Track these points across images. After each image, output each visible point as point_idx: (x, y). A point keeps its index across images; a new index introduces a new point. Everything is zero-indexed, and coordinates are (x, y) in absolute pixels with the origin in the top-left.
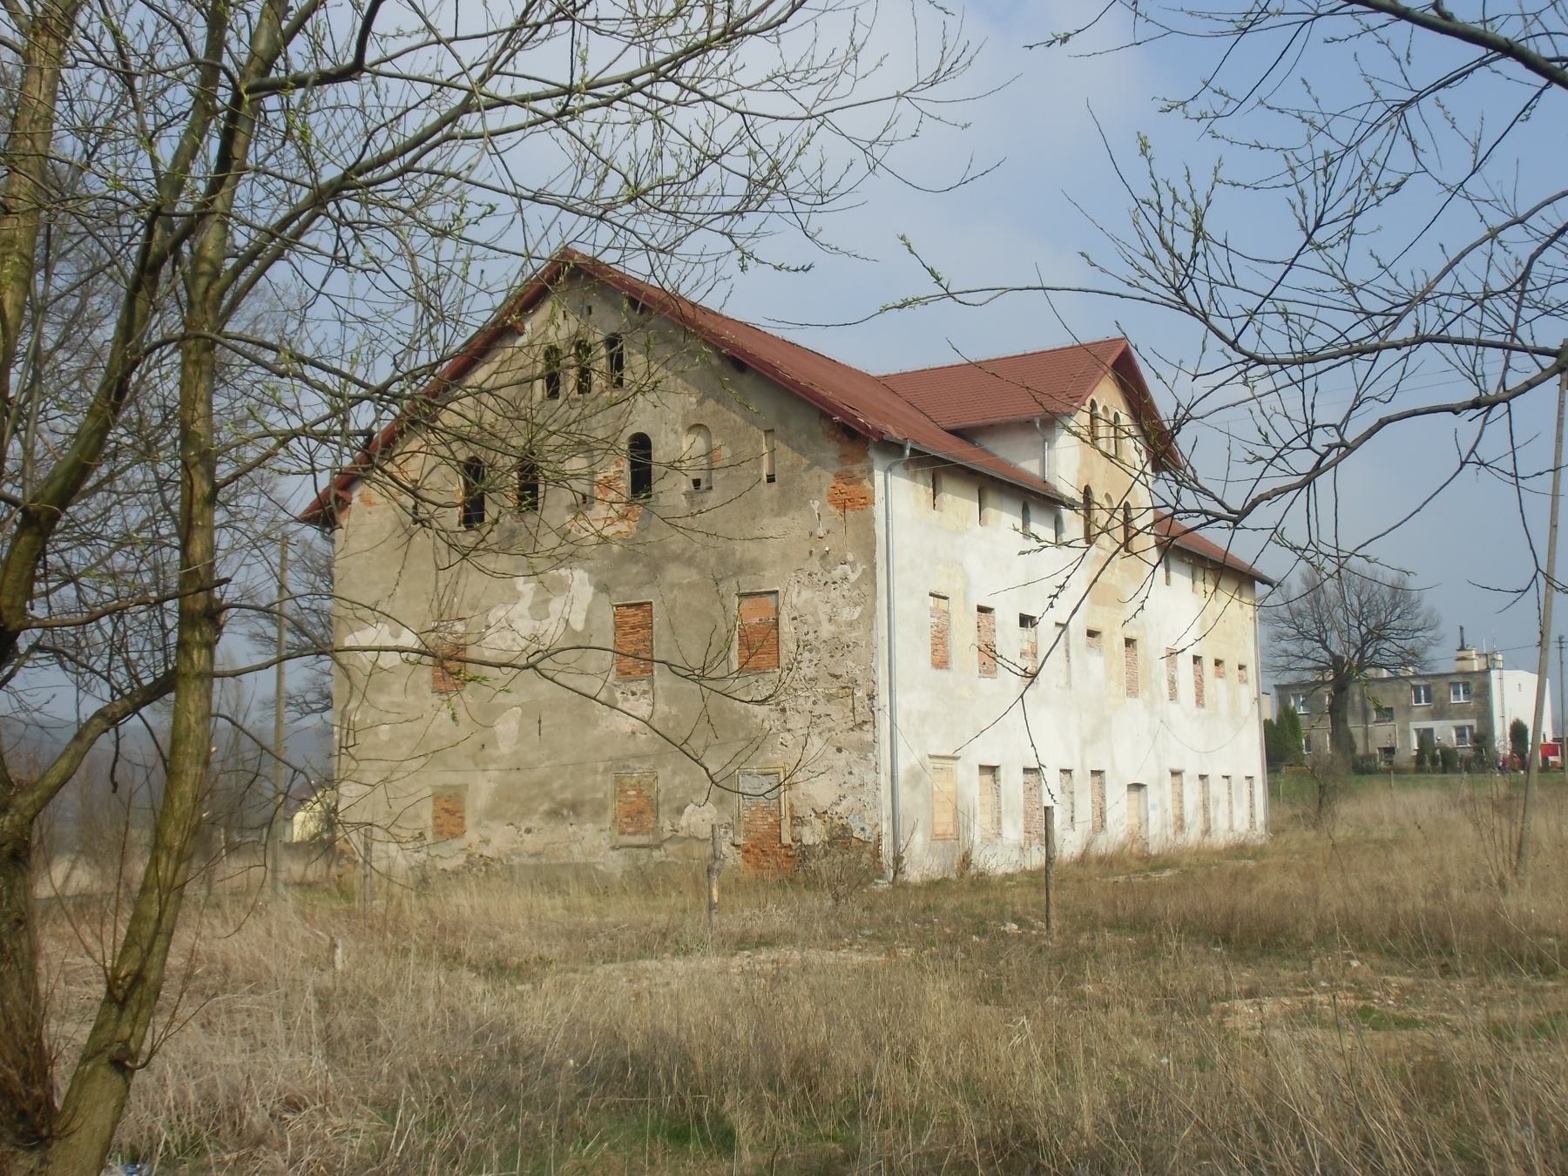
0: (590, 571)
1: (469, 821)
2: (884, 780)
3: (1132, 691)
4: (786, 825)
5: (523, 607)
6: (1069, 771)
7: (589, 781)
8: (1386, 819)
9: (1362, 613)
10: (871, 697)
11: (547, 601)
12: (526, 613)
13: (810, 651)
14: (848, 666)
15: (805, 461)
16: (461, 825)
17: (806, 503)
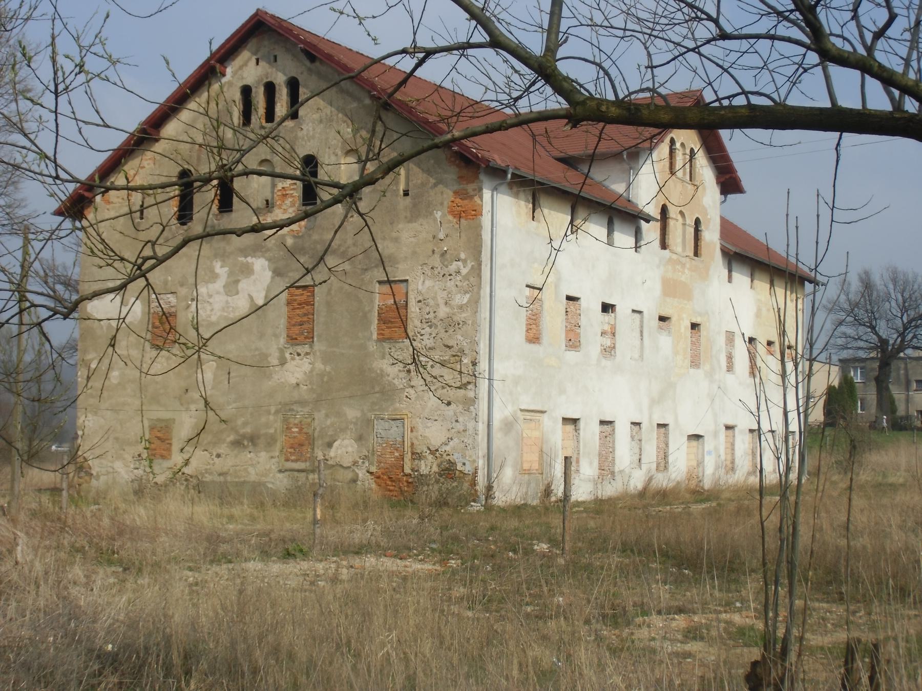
0: (269, 260)
1: (176, 448)
2: (482, 427)
3: (695, 363)
4: (408, 457)
5: (219, 285)
6: (639, 424)
7: (263, 420)
8: (902, 469)
9: (904, 306)
10: (474, 364)
11: (237, 282)
12: (222, 290)
13: (430, 327)
14: (458, 339)
15: (432, 181)
16: (169, 450)
17: (431, 214)
